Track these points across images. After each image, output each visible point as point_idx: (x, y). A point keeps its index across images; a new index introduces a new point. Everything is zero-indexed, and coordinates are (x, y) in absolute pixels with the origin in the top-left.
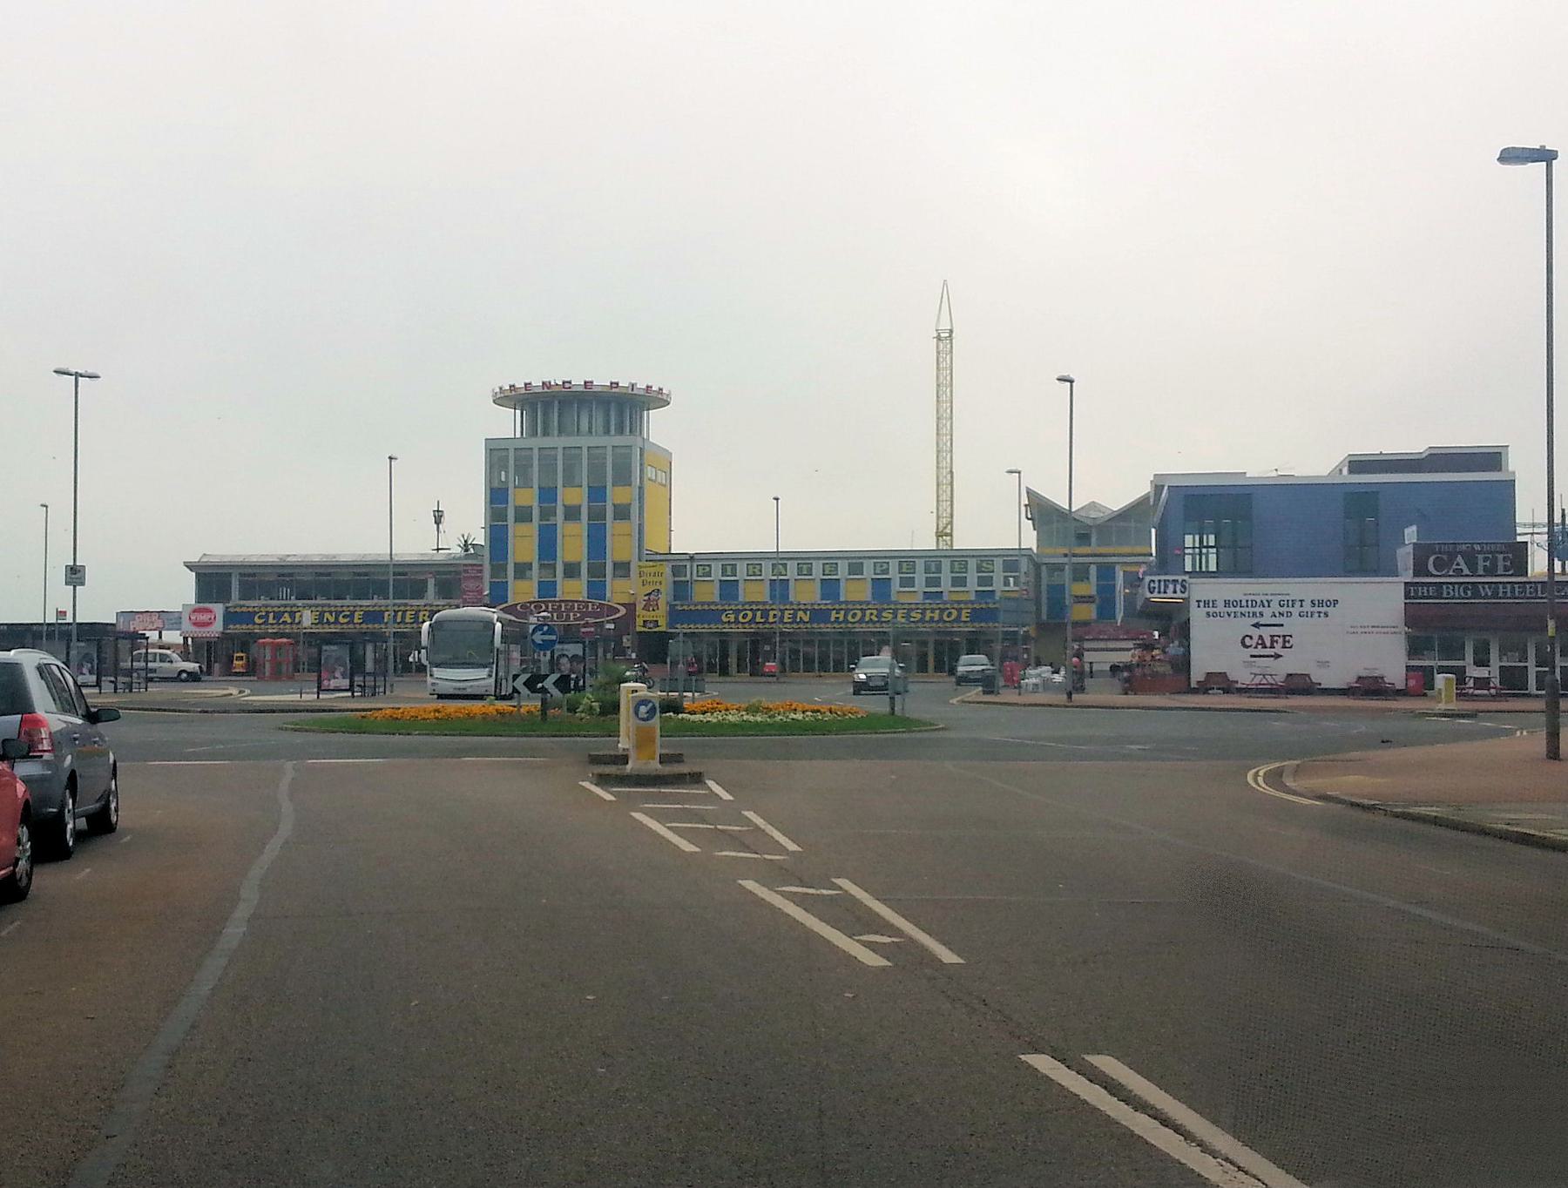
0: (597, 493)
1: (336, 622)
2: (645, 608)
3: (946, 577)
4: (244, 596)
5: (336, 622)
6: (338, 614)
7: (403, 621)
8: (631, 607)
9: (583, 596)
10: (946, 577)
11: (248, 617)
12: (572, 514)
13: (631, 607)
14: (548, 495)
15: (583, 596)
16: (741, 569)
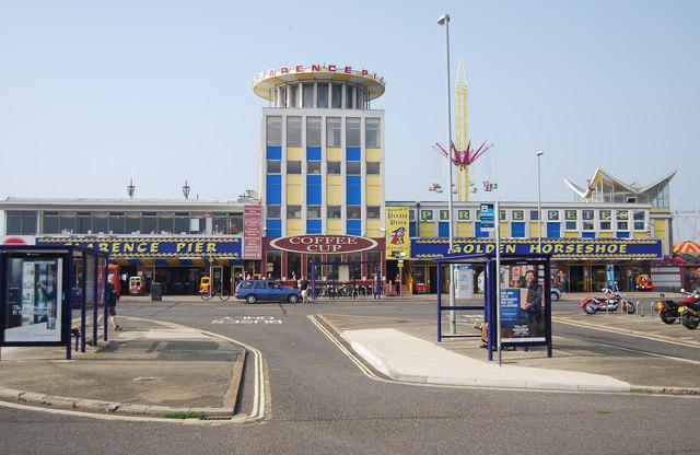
0: (353, 153)
1: (135, 251)
2: (394, 241)
3: (596, 222)
4: (47, 230)
6: (136, 244)
7: (193, 250)
8: (382, 241)
9: (343, 232)
10: (596, 222)
12: (334, 168)
13: (382, 241)
14: (313, 153)
15: (343, 232)
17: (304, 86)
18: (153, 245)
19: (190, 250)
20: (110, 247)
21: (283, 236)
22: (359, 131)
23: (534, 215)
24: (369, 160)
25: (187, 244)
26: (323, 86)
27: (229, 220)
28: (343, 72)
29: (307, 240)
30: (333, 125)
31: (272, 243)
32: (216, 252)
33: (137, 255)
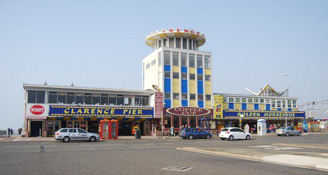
1: (103, 113)
2: (217, 111)
5: (103, 113)
6: (103, 110)
7: (131, 114)
8: (212, 110)
10: (281, 105)
11: (61, 110)
12: (192, 77)
13: (212, 110)
14: (184, 69)
16: (234, 99)
17: (177, 39)
18: (112, 110)
19: (130, 113)
20: (90, 111)
21: (172, 108)
22: (170, 57)
23: (238, 100)
24: (191, 73)
25: (128, 110)
26: (171, 39)
27: (143, 99)
28: (190, 33)
29: (182, 109)
30: (184, 55)
31: (167, 111)
32: (142, 115)
33: (71, 115)
